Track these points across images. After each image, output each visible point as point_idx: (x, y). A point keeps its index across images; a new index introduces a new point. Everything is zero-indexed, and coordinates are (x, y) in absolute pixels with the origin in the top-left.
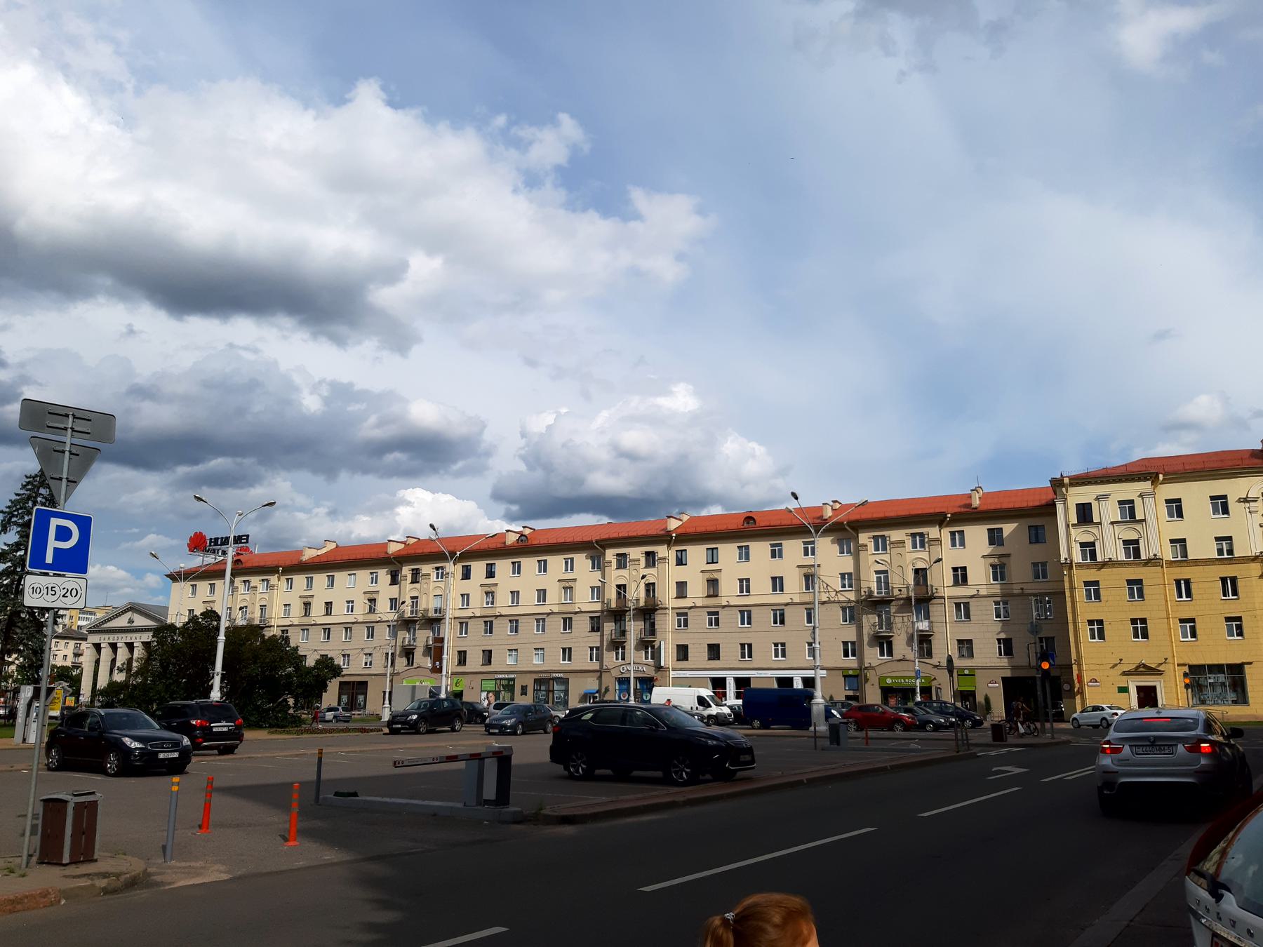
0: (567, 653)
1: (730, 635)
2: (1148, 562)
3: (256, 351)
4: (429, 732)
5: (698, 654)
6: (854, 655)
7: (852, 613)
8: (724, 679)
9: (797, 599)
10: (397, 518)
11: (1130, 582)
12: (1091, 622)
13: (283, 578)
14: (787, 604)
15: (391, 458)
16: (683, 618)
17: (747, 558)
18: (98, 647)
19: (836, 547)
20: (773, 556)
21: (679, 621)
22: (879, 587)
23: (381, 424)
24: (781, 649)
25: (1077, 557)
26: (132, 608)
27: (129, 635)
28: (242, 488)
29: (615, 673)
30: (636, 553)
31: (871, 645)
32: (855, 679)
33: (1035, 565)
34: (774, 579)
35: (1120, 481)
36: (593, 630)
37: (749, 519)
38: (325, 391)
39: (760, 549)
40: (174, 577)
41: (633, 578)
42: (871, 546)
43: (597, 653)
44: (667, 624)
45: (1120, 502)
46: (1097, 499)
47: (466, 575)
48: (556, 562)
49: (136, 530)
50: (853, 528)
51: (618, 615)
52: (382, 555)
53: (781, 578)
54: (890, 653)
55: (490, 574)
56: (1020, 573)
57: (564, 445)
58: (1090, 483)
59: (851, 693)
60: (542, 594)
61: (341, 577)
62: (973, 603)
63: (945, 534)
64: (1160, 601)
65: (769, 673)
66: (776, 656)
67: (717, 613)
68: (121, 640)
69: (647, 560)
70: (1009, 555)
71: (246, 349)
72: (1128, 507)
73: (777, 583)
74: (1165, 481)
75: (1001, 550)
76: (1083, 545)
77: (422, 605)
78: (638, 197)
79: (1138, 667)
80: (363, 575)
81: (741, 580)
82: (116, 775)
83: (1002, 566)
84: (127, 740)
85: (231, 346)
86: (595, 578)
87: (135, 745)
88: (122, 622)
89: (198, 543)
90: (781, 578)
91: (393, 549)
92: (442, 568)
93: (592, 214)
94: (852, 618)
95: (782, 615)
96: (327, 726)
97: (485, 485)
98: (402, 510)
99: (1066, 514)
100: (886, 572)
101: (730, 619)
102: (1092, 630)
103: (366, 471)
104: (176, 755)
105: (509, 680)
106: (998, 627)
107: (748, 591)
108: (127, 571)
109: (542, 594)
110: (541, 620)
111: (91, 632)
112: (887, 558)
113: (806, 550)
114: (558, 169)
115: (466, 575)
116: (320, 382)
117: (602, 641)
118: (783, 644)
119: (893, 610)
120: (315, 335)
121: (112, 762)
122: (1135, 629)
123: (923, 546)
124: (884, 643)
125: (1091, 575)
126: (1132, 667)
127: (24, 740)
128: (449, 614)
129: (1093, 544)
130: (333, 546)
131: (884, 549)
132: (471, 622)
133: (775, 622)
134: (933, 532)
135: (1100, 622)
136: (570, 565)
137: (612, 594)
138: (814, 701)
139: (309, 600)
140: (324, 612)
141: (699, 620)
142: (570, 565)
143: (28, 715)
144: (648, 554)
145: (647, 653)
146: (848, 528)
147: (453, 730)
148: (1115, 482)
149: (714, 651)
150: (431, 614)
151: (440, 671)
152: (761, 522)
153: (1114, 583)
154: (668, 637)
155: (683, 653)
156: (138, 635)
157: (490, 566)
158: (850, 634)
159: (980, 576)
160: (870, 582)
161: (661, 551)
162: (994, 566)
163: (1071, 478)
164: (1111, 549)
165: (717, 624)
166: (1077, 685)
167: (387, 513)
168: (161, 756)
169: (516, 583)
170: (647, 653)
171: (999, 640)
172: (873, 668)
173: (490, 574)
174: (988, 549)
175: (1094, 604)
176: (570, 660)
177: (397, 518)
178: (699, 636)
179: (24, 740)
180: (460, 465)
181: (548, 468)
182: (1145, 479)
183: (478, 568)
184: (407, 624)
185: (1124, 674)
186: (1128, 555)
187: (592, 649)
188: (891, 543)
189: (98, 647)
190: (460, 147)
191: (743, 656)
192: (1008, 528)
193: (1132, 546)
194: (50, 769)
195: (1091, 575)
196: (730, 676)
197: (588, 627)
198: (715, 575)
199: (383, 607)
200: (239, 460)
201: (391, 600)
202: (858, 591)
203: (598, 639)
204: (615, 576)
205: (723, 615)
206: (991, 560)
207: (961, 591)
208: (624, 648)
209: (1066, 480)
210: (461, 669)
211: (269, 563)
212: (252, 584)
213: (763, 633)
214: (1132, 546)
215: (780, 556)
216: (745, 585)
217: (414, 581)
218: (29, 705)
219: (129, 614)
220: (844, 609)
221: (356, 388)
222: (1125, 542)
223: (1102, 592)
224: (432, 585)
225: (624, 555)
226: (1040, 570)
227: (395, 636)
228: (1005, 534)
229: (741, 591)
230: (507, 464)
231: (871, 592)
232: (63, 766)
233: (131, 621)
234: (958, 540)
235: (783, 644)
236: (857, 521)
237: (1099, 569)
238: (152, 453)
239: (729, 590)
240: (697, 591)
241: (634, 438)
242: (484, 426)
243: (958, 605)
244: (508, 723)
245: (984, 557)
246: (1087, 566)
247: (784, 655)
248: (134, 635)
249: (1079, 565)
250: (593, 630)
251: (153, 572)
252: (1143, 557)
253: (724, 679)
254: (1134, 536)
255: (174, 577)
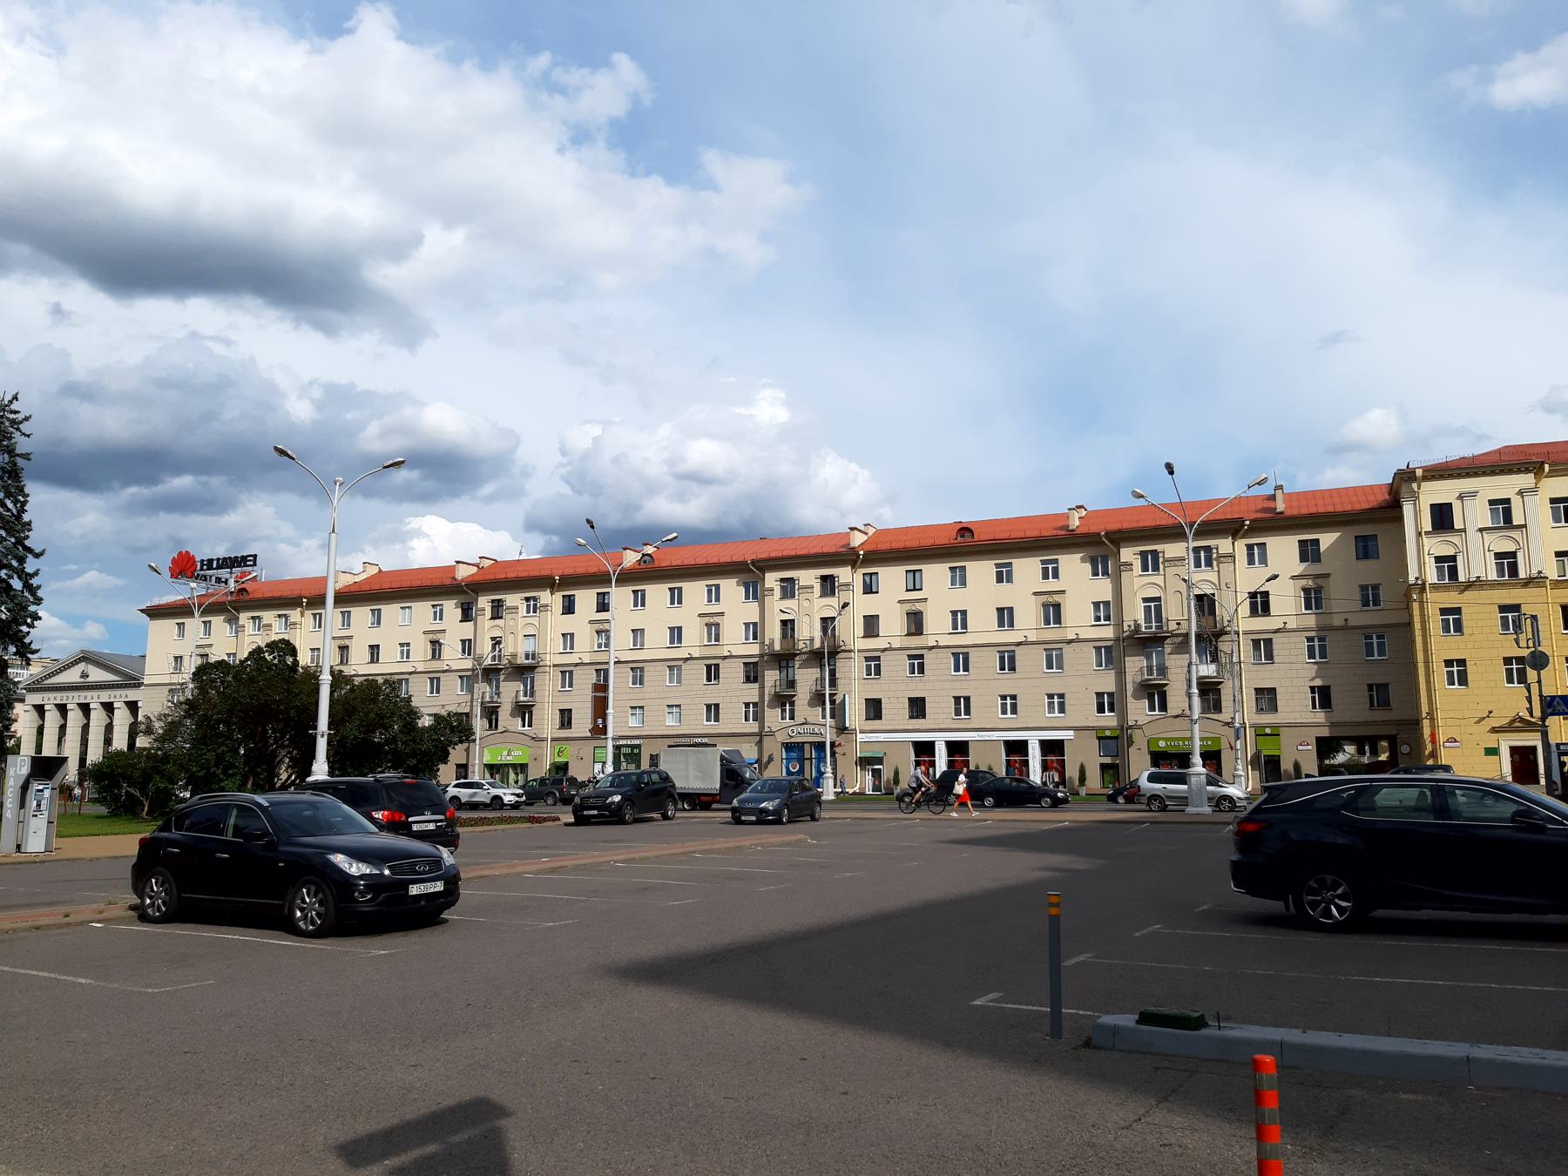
0: (713, 710)
1: (939, 686)
2: (1530, 582)
3: (228, 343)
4: (637, 821)
5: (895, 711)
6: (1111, 709)
7: (1111, 654)
8: (1026, 742)
9: (1032, 637)
10: (410, 554)
11: (1504, 608)
12: (1449, 663)
13: (308, 613)
14: (1019, 644)
15: (402, 475)
16: (874, 664)
17: (964, 583)
18: (40, 710)
19: (1088, 567)
20: (1000, 579)
21: (869, 668)
22: (1148, 619)
23: (385, 434)
24: (1010, 703)
25: (1432, 577)
26: (86, 658)
27: (83, 694)
28: (212, 513)
29: (782, 737)
30: (808, 577)
31: (1136, 697)
32: (1115, 743)
33: (1364, 588)
34: (1000, 610)
35: (1493, 473)
36: (748, 680)
37: (965, 530)
38: (317, 393)
39: (981, 571)
40: (155, 613)
41: (809, 613)
42: (1137, 564)
43: (755, 711)
44: (852, 671)
45: (1492, 502)
46: (1461, 497)
47: (569, 608)
48: (695, 590)
49: (73, 567)
50: (1112, 541)
51: (783, 659)
52: (448, 582)
53: (1011, 610)
54: (1163, 707)
55: (603, 606)
56: (1343, 601)
57: (615, 461)
58: (1451, 477)
59: (1108, 760)
60: (676, 634)
61: (390, 611)
62: (1277, 639)
63: (1241, 546)
64: (939, 686)
65: (995, 736)
66: (1004, 712)
67: (922, 657)
68: (72, 700)
69: (823, 587)
70: (1328, 576)
71: (213, 338)
72: (1502, 508)
73: (1005, 616)
74: (1554, 473)
75: (1317, 569)
76: (1439, 559)
77: (508, 648)
78: (713, 161)
79: (1513, 721)
80: (422, 610)
81: (954, 613)
82: (318, 934)
83: (1318, 590)
84: (339, 859)
85: (194, 335)
86: (751, 611)
87: (355, 869)
88: (72, 676)
89: (184, 567)
90: (1011, 610)
91: (463, 573)
92: (535, 599)
93: (656, 180)
94: (1109, 661)
95: (1012, 659)
96: (506, 814)
97: (517, 512)
98: (415, 543)
99: (1416, 517)
100: (1159, 599)
101: (939, 664)
102: (1450, 674)
103: (368, 494)
104: (439, 886)
105: (633, 747)
106: (1312, 670)
107: (964, 626)
108: (61, 618)
109: (676, 634)
110: (674, 666)
111: (30, 690)
112: (1159, 580)
113: (1045, 571)
114: (614, 123)
115: (569, 608)
116: (311, 384)
117: (762, 695)
118: (1014, 697)
119: (1168, 649)
120: (297, 322)
121: (307, 905)
122: (1509, 672)
123: (1209, 563)
124: (1155, 693)
125: (1451, 599)
126: (1504, 722)
127: (19, 847)
128: (550, 660)
129: (1453, 558)
130: (375, 570)
131: (1156, 568)
132: (577, 671)
133: (1002, 668)
134: (1224, 545)
135: (1462, 662)
136: (714, 594)
137: (774, 633)
138: (1192, 770)
139: (347, 642)
140: (368, 659)
141: (895, 666)
142: (714, 594)
143: (22, 805)
144: (824, 578)
145: (783, 711)
146: (1101, 543)
147: (665, 817)
148: (1485, 474)
149: (917, 707)
150: (521, 660)
151: (604, 730)
152: (981, 536)
153: (1480, 612)
154: (854, 688)
155: (874, 708)
156: (95, 693)
157: (602, 596)
158: (1108, 683)
159: (1287, 604)
160: (1135, 613)
161: (843, 574)
162: (1306, 590)
163: (1426, 469)
164: (1478, 562)
165: (922, 671)
166: (1429, 747)
167: (398, 547)
168: (414, 890)
169: (639, 619)
170: (783, 711)
171: (1312, 689)
172: (1140, 727)
173: (603, 606)
174: (1300, 568)
175: (1454, 638)
176: (717, 720)
177: (410, 554)
178: (895, 688)
179: (19, 847)
180: (488, 489)
181: (597, 490)
182: (1527, 471)
183: (586, 598)
184: (490, 673)
185: (1494, 730)
186: (1501, 572)
187: (747, 705)
188: (1165, 561)
189: (40, 710)
190: (493, 92)
191: (958, 713)
192: (1327, 539)
193: (1507, 562)
194: (144, 918)
195: (1451, 599)
196: (940, 741)
197: (741, 675)
198: (918, 606)
199: (453, 656)
200: (203, 478)
201: (463, 642)
202: (1119, 625)
203: (756, 692)
204: (777, 608)
205: (886, 660)
206: (1303, 582)
207: (1261, 623)
208: (792, 704)
209: (1419, 473)
210: (565, 733)
211: (287, 593)
212: (265, 621)
213: (985, 683)
214: (1507, 562)
215: (1010, 580)
216: (960, 619)
217: (496, 615)
218: (25, 788)
219: (82, 666)
220: (1098, 649)
221: (359, 389)
222: (1498, 556)
223: (1465, 624)
224: (521, 622)
225: (791, 580)
226: (1370, 595)
227: (471, 690)
228: (1323, 548)
229: (955, 627)
230: (547, 488)
231: (1137, 626)
232: (178, 913)
233: (85, 675)
234: (1257, 555)
235: (1014, 697)
236: (1119, 531)
237: (1462, 592)
238: (92, 469)
239: (937, 626)
240: (893, 627)
241: (704, 453)
242: (518, 443)
243: (1256, 643)
244: (768, 805)
245: (1293, 577)
246: (1502, 585)
247: (1014, 711)
248: (89, 694)
249: (1435, 587)
250: (748, 680)
251: (96, 620)
252: (1522, 575)
253: (1026, 742)
254: (1511, 547)
255: (155, 613)
